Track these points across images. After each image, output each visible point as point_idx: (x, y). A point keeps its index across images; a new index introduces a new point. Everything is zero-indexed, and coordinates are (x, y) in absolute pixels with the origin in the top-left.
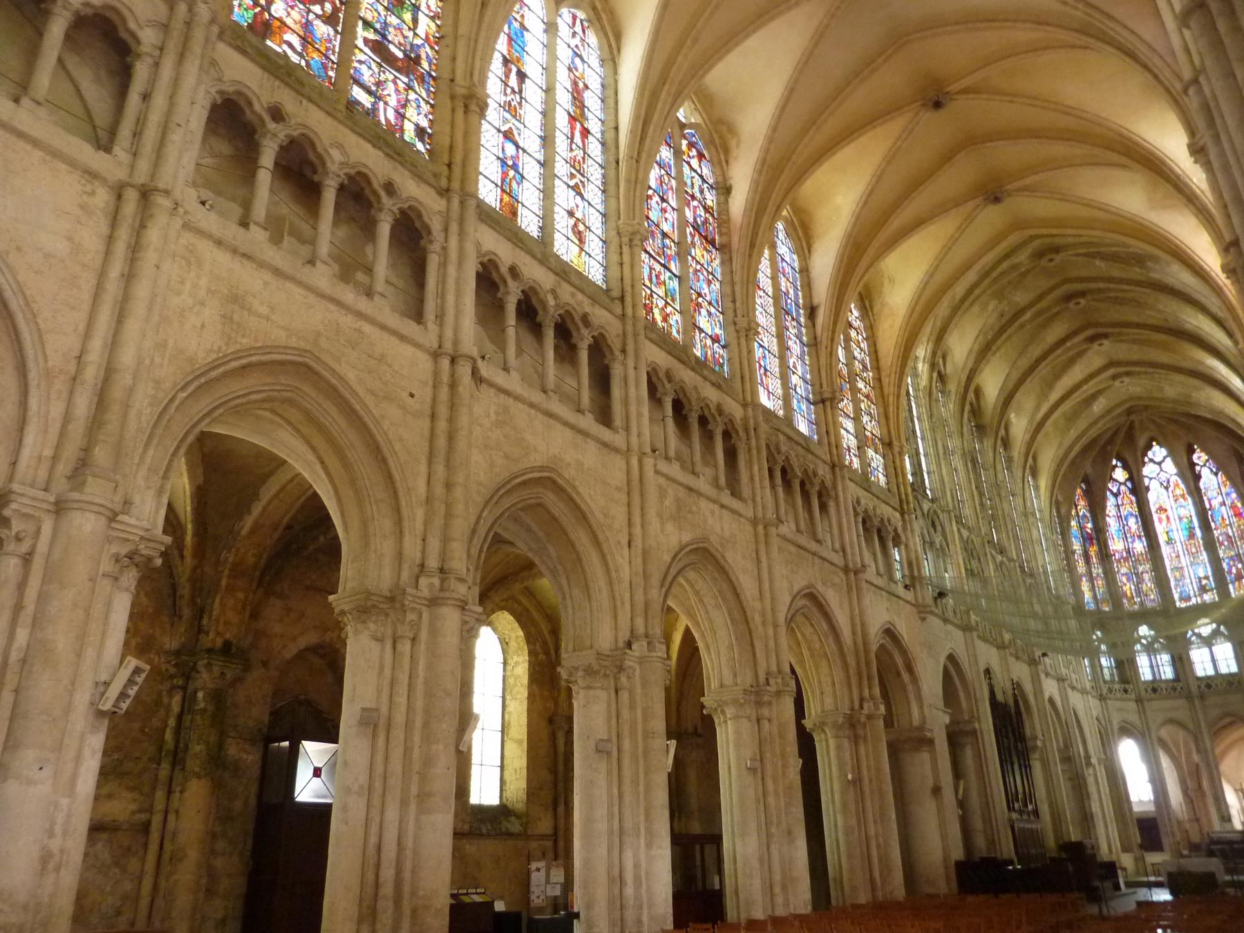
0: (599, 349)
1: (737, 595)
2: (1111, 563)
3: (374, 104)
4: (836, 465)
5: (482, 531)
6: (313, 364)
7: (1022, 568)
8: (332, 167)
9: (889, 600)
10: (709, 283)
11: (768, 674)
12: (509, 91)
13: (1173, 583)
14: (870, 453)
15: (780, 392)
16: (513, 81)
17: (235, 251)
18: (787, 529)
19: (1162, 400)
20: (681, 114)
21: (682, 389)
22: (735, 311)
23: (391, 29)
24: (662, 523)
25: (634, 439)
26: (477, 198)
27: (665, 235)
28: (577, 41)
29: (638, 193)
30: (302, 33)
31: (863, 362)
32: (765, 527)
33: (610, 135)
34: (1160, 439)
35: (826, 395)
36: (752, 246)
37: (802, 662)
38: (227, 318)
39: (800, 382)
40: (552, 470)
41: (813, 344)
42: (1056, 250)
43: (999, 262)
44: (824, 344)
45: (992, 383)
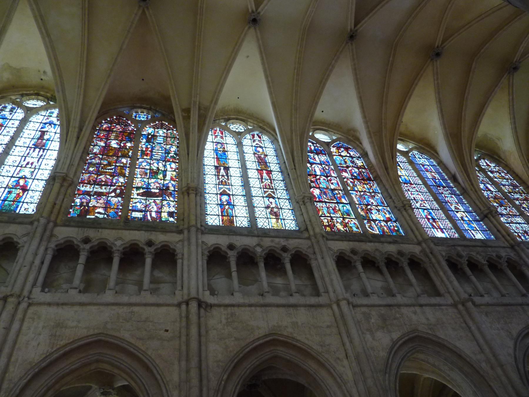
1: (460, 357)
16: (222, 172)
17: (58, 304)
22: (393, 201)
29: (300, 181)
32: (463, 305)
35: (487, 212)
44: (469, 189)
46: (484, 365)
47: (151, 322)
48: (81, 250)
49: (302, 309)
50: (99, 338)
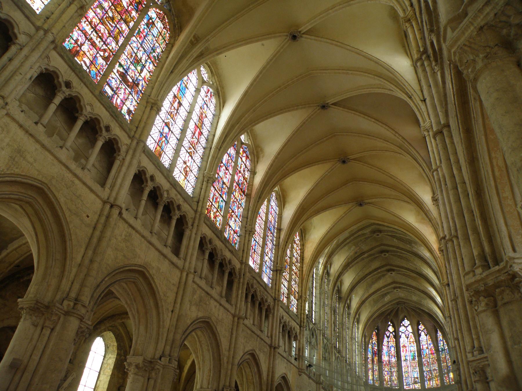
0: (181, 222)
2: (382, 365)
3: (113, 95)
4: (276, 300)
5: (103, 287)
6: (46, 190)
7: (346, 361)
8: (84, 112)
9: (287, 364)
10: (239, 208)
11: (224, 386)
12: (173, 108)
14: (292, 298)
15: (259, 262)
16: (176, 105)
17: (27, 132)
18: (249, 322)
19: (411, 301)
20: (243, 137)
21: (215, 249)
22: (247, 222)
23: (130, 70)
24: (191, 306)
25: (187, 264)
26: (145, 144)
27: (224, 183)
28: (207, 99)
30: (92, 60)
31: (297, 259)
32: (238, 319)
33: (211, 138)
34: (408, 318)
35: (279, 268)
36: (260, 198)
37: (242, 385)
38: (12, 158)
39: (268, 260)
40: (145, 268)
41: (277, 246)
42: (380, 231)
43: (359, 231)
45: (348, 281)
46: (225, 358)
47: (82, 201)
48: (61, 92)
49: (167, 261)
50: (43, 187)
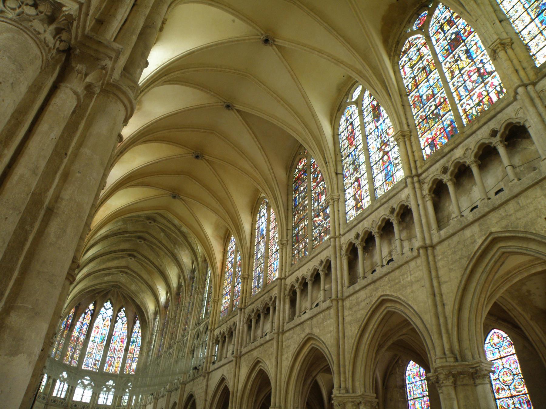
13: (85, 358)
19: (128, 289)
35: (246, 276)
